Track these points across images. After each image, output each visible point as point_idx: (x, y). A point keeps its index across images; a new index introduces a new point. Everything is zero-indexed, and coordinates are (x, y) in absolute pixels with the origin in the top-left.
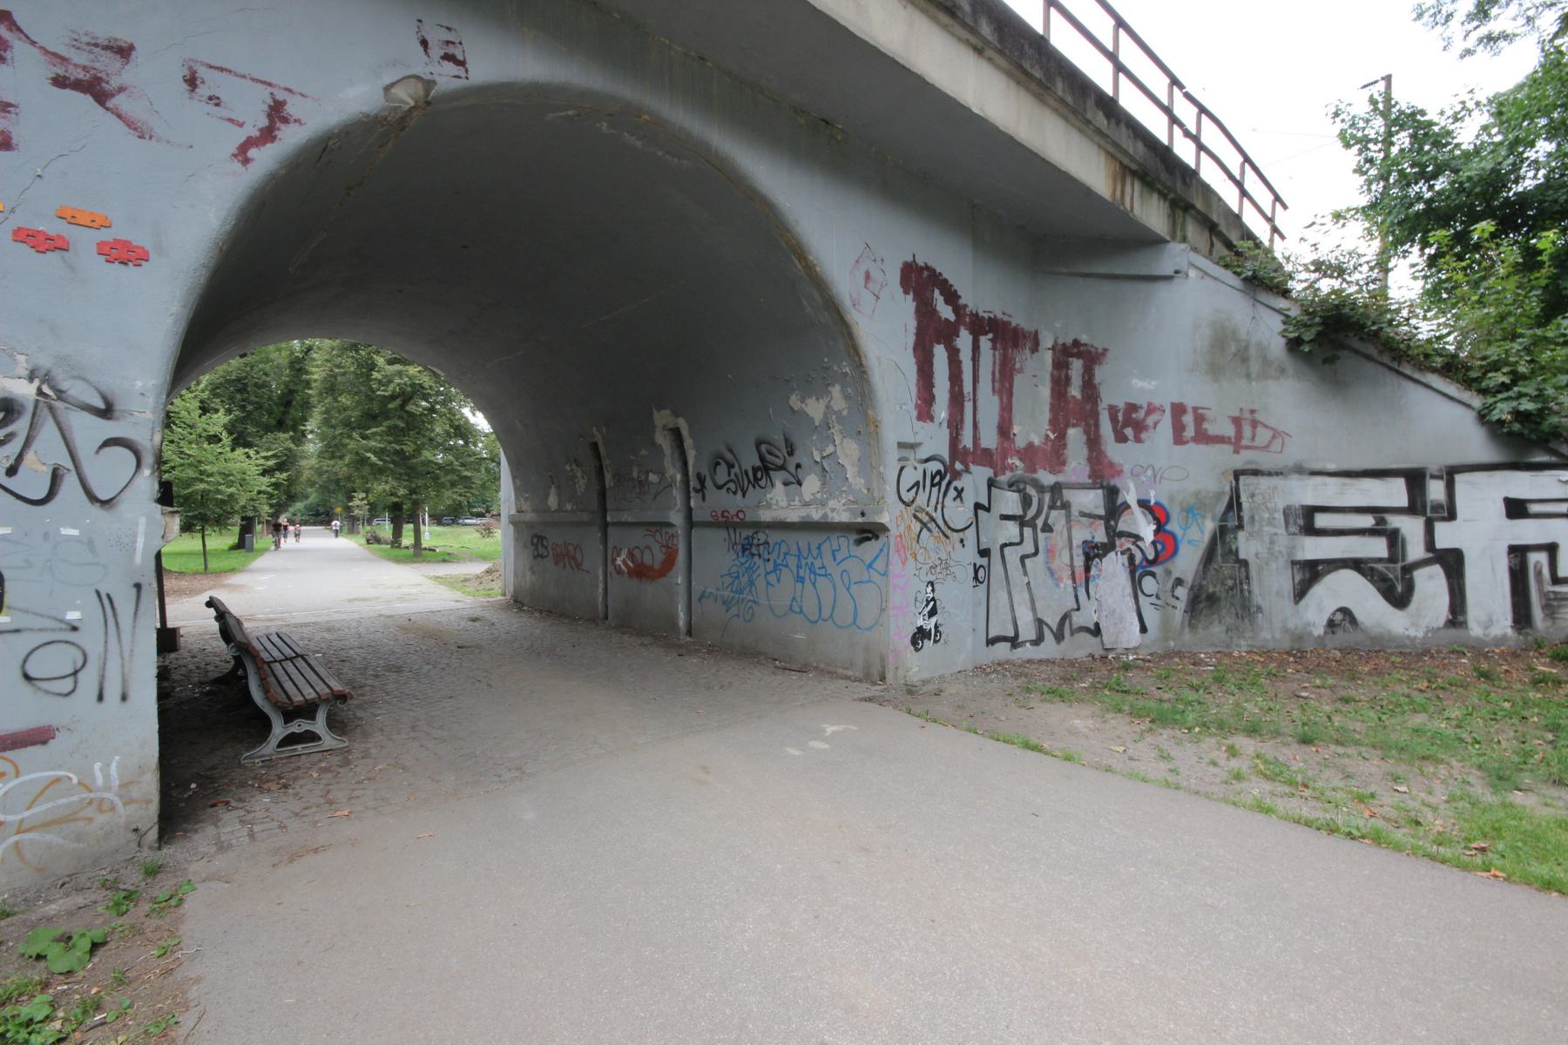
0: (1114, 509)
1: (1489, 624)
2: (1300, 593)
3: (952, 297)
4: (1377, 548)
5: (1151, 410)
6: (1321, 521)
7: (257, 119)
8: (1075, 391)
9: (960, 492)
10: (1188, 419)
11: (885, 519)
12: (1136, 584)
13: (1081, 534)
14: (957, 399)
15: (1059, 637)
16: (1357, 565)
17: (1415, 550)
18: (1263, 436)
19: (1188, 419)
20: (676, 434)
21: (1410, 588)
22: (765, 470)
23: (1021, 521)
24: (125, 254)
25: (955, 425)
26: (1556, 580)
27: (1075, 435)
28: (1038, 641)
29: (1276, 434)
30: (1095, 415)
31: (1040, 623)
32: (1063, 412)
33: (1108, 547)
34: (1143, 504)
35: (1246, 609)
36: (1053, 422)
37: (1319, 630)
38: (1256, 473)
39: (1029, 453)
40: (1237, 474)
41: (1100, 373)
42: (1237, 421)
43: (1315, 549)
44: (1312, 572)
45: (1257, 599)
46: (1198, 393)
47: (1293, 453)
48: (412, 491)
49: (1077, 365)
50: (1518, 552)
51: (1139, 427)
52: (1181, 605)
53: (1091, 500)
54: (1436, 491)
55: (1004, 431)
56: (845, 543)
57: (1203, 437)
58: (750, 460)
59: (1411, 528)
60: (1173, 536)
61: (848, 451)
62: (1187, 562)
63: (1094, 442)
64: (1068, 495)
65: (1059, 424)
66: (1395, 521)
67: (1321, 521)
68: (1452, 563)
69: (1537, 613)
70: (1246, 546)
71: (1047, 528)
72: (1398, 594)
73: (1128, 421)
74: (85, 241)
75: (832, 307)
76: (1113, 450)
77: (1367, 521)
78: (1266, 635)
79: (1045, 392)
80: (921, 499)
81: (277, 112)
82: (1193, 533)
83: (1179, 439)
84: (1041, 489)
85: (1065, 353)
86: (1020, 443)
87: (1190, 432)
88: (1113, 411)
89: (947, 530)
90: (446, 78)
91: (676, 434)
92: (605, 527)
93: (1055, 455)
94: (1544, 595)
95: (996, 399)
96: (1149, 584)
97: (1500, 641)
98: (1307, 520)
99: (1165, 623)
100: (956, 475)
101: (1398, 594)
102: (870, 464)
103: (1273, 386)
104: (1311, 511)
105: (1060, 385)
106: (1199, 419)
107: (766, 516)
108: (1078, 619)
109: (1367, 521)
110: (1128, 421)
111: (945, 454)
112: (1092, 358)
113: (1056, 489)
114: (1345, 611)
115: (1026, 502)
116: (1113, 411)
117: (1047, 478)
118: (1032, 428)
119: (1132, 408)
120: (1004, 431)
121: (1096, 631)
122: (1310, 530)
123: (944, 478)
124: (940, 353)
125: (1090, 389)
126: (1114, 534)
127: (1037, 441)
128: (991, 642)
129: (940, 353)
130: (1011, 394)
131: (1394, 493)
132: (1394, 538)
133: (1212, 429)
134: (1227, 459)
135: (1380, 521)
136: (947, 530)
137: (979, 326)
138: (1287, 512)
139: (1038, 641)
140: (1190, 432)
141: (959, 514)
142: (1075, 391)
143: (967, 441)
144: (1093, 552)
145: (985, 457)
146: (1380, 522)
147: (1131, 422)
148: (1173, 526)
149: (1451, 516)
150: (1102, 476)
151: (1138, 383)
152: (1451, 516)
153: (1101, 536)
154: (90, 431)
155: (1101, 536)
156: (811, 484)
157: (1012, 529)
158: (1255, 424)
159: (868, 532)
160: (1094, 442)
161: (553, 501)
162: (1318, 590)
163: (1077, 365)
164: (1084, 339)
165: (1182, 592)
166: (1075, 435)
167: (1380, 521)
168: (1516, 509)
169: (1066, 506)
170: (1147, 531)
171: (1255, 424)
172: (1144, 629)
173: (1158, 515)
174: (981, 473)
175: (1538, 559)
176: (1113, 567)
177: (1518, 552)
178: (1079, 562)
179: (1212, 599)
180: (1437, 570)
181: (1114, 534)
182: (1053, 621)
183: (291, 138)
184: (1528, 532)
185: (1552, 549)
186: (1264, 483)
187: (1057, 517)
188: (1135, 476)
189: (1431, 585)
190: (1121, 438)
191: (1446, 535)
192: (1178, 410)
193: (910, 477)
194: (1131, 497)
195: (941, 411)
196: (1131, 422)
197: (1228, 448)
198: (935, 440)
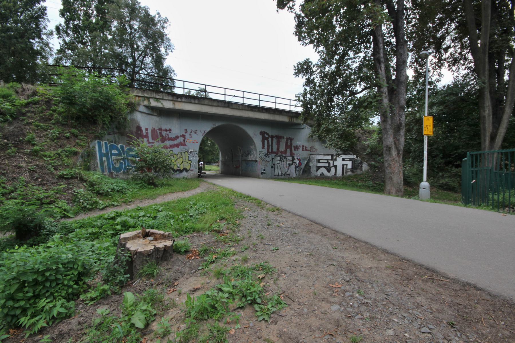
0: (293, 159)
1: (339, 175)
2: (317, 170)
3: (268, 134)
4: (327, 165)
5: (299, 146)
6: (321, 161)
7: (203, 133)
8: (289, 144)
9: (269, 157)
10: (304, 147)
11: (257, 160)
12: (296, 169)
13: (288, 163)
14: (268, 146)
15: (284, 175)
16: (324, 167)
17: (331, 165)
18: (314, 150)
19: (304, 147)
20: (240, 149)
21: (330, 170)
22: (248, 154)
23: (280, 161)
24: (197, 142)
25: (268, 149)
26: (347, 169)
27: (288, 150)
28: (282, 175)
29: (316, 149)
30: (291, 147)
31: (282, 174)
32: (287, 147)
33: (292, 164)
34: (297, 159)
35: (310, 172)
36: (285, 148)
37: (319, 175)
38: (313, 155)
39: (282, 152)
40: (310, 155)
41: (293, 141)
42: (311, 148)
43: (320, 165)
44: (319, 168)
45: (312, 171)
46: (306, 144)
47: (318, 152)
48: (203, 156)
49: (289, 141)
50: (343, 165)
51: (298, 149)
52: (301, 172)
53: (290, 158)
54: (335, 157)
55: (278, 149)
56: (254, 162)
57: (306, 150)
58: (247, 153)
59: (331, 162)
60: (301, 163)
61: (255, 152)
62: (303, 166)
63: (291, 151)
64: (287, 157)
65: (286, 148)
66: (329, 161)
67: (321, 161)
68: (335, 167)
69: (345, 173)
70: (311, 164)
71: (284, 162)
72: (329, 170)
73: (296, 148)
74: (195, 142)
75: (251, 137)
76: (294, 152)
77: (326, 161)
78: (312, 176)
79: (285, 144)
80: (263, 158)
81: (204, 132)
82: (304, 162)
83: (303, 150)
84: (283, 156)
85: (287, 139)
86: (280, 151)
87: (304, 149)
88: (294, 146)
89: (266, 161)
90: (214, 126)
91: (240, 149)
92: (233, 161)
93: (285, 152)
94: (346, 171)
95: (276, 146)
96: (297, 169)
97: (340, 177)
98: (319, 161)
99: (299, 174)
100: (268, 155)
101: (329, 170)
102: (256, 153)
103: (316, 143)
104: (319, 160)
105: (287, 143)
106: (306, 147)
107: (248, 159)
108: (287, 173)
109: (326, 161)
110: (296, 148)
111: (267, 153)
112: (291, 139)
113: (285, 157)
114: (322, 173)
115: (281, 158)
116: (294, 146)
117: (284, 155)
118: (282, 148)
119: (297, 146)
120: (278, 149)
121: (289, 175)
122: (319, 162)
123: (267, 155)
124: (266, 141)
125: (291, 144)
126: (293, 162)
127: (283, 150)
128: (275, 175)
129: (266, 141)
130: (279, 144)
131: (330, 157)
132: (329, 164)
133: (307, 149)
134: (309, 152)
135: (328, 161)
136: (266, 161)
137: (272, 137)
138: (316, 160)
139: (282, 175)
140: (304, 149)
141: (268, 159)
142: (289, 144)
143: (270, 150)
144: (290, 165)
145: (274, 153)
146: (328, 161)
147: (297, 148)
148: (301, 162)
149: (336, 161)
150: (292, 155)
151: (298, 143)
152: (336, 161)
153: (291, 163)
154: (195, 153)
155: (291, 163)
156: (252, 156)
157: (279, 162)
158: (313, 148)
159: (256, 161)
160: (291, 151)
161: (226, 158)
162: (319, 170)
163: (289, 141)
164: (291, 137)
165: (302, 170)
166: (288, 150)
167: (328, 161)
168: (343, 160)
169: (286, 159)
170: (298, 162)
171: (313, 148)
172: (296, 175)
173: (299, 160)
174: (273, 155)
175: (345, 166)
176: (293, 167)
177: (343, 165)
178: (288, 166)
179: (306, 171)
180: (334, 168)
181: (293, 162)
182: (284, 173)
183: (205, 133)
184: (345, 163)
185: (347, 165)
186: (314, 156)
187: (285, 160)
188: (296, 155)
189: (333, 169)
190: (295, 150)
191: (335, 163)
192: (303, 146)
193: (261, 155)
194: (296, 158)
195: (266, 147)
196: (297, 148)
197: (309, 151)
198: (265, 151)
